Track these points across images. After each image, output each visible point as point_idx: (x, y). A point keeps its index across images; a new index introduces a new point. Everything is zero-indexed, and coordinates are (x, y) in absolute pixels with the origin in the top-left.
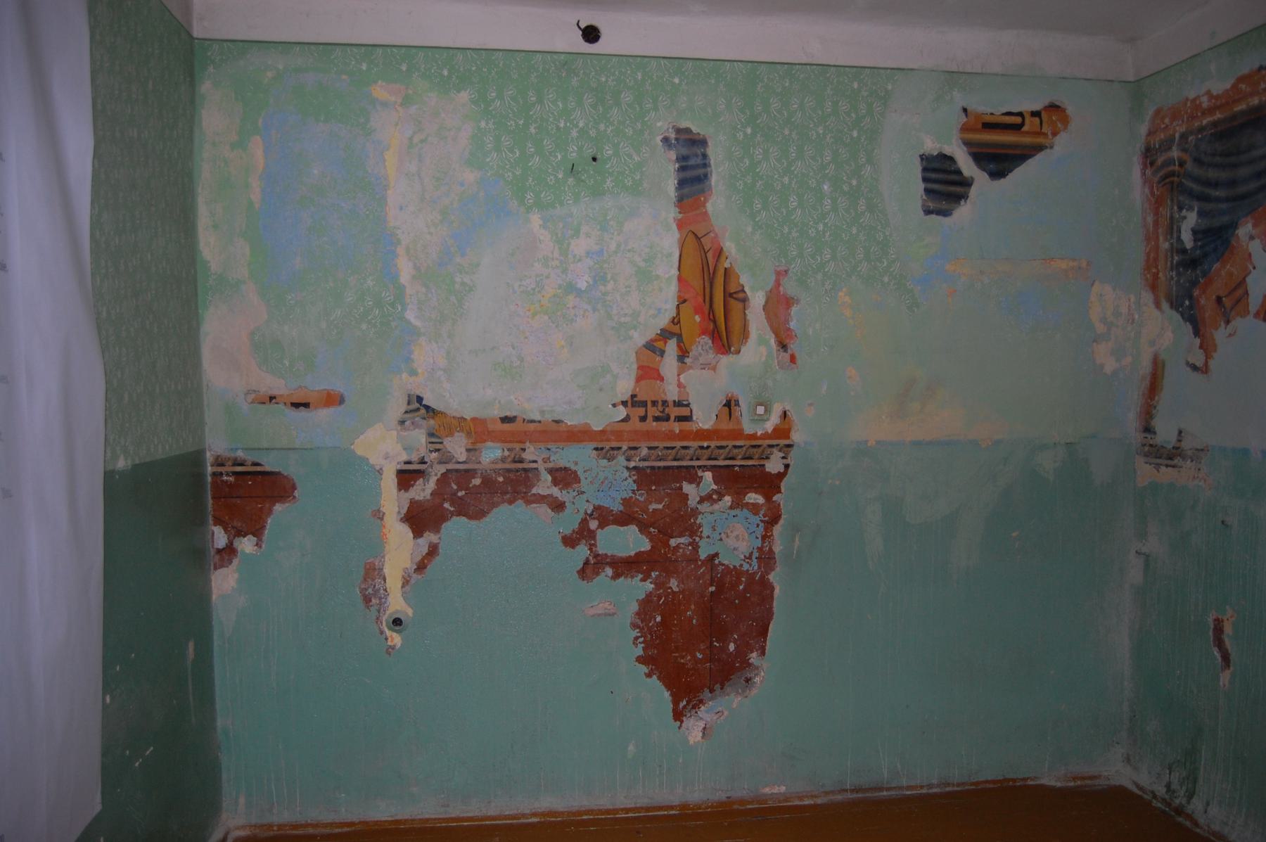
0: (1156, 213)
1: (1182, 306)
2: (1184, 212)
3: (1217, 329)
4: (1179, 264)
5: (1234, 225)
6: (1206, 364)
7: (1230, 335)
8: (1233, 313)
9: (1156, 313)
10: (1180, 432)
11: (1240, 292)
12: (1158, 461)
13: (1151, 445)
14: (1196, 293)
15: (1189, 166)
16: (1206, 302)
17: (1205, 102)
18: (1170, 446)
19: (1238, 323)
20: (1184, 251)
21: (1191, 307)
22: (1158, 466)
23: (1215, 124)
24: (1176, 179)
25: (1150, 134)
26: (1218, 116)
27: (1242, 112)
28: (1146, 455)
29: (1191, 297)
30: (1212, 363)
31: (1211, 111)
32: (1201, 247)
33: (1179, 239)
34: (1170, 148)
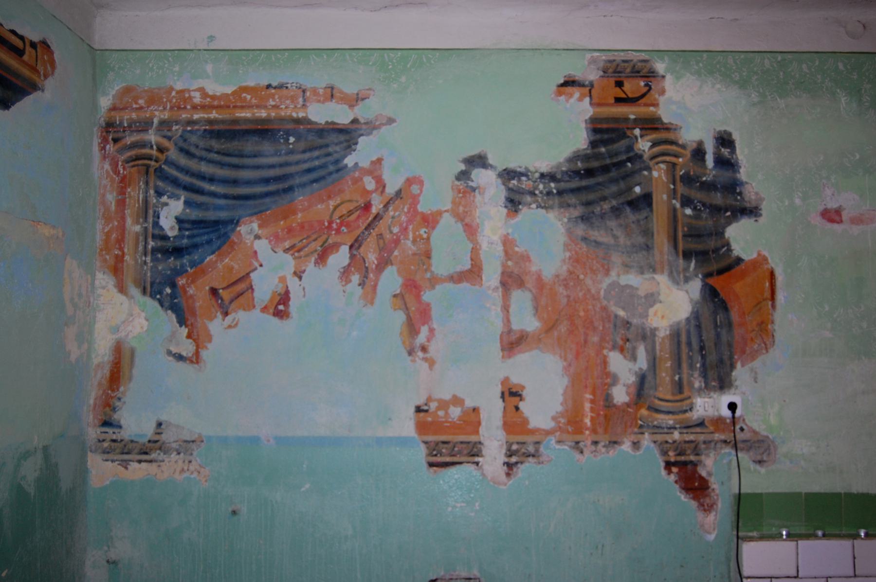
0: (122, 192)
1: (160, 293)
2: (165, 199)
3: (211, 320)
4: (154, 250)
5: (234, 222)
6: (197, 353)
7: (230, 327)
8: (233, 306)
9: (122, 298)
10: (159, 424)
11: (241, 286)
12: (126, 457)
13: (114, 441)
14: (181, 281)
15: (173, 154)
16: (197, 292)
17: (197, 98)
18: (145, 440)
19: (241, 315)
20: (165, 238)
21: (173, 296)
22: (125, 464)
23: (210, 122)
24: (153, 163)
25: (114, 108)
26: (214, 115)
27: (247, 121)
28: (105, 452)
29: (173, 285)
30: (204, 354)
31: (203, 107)
32: (189, 237)
33: (156, 224)
34: (145, 130)
